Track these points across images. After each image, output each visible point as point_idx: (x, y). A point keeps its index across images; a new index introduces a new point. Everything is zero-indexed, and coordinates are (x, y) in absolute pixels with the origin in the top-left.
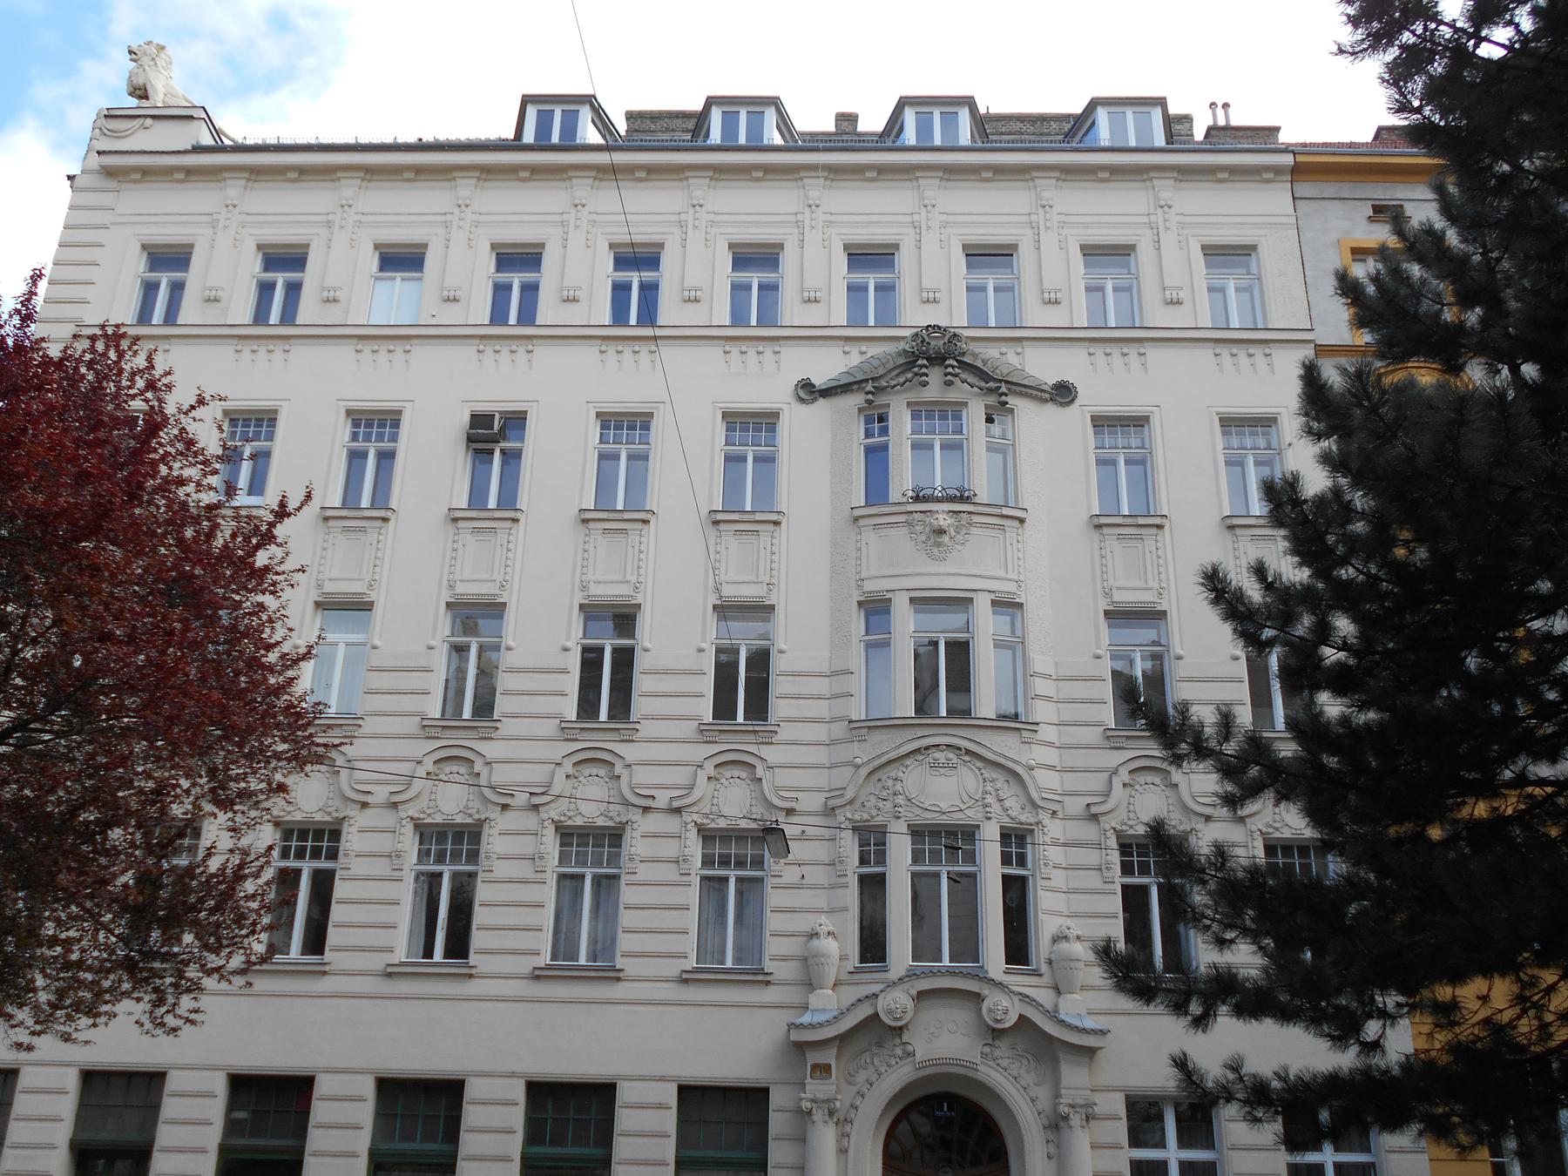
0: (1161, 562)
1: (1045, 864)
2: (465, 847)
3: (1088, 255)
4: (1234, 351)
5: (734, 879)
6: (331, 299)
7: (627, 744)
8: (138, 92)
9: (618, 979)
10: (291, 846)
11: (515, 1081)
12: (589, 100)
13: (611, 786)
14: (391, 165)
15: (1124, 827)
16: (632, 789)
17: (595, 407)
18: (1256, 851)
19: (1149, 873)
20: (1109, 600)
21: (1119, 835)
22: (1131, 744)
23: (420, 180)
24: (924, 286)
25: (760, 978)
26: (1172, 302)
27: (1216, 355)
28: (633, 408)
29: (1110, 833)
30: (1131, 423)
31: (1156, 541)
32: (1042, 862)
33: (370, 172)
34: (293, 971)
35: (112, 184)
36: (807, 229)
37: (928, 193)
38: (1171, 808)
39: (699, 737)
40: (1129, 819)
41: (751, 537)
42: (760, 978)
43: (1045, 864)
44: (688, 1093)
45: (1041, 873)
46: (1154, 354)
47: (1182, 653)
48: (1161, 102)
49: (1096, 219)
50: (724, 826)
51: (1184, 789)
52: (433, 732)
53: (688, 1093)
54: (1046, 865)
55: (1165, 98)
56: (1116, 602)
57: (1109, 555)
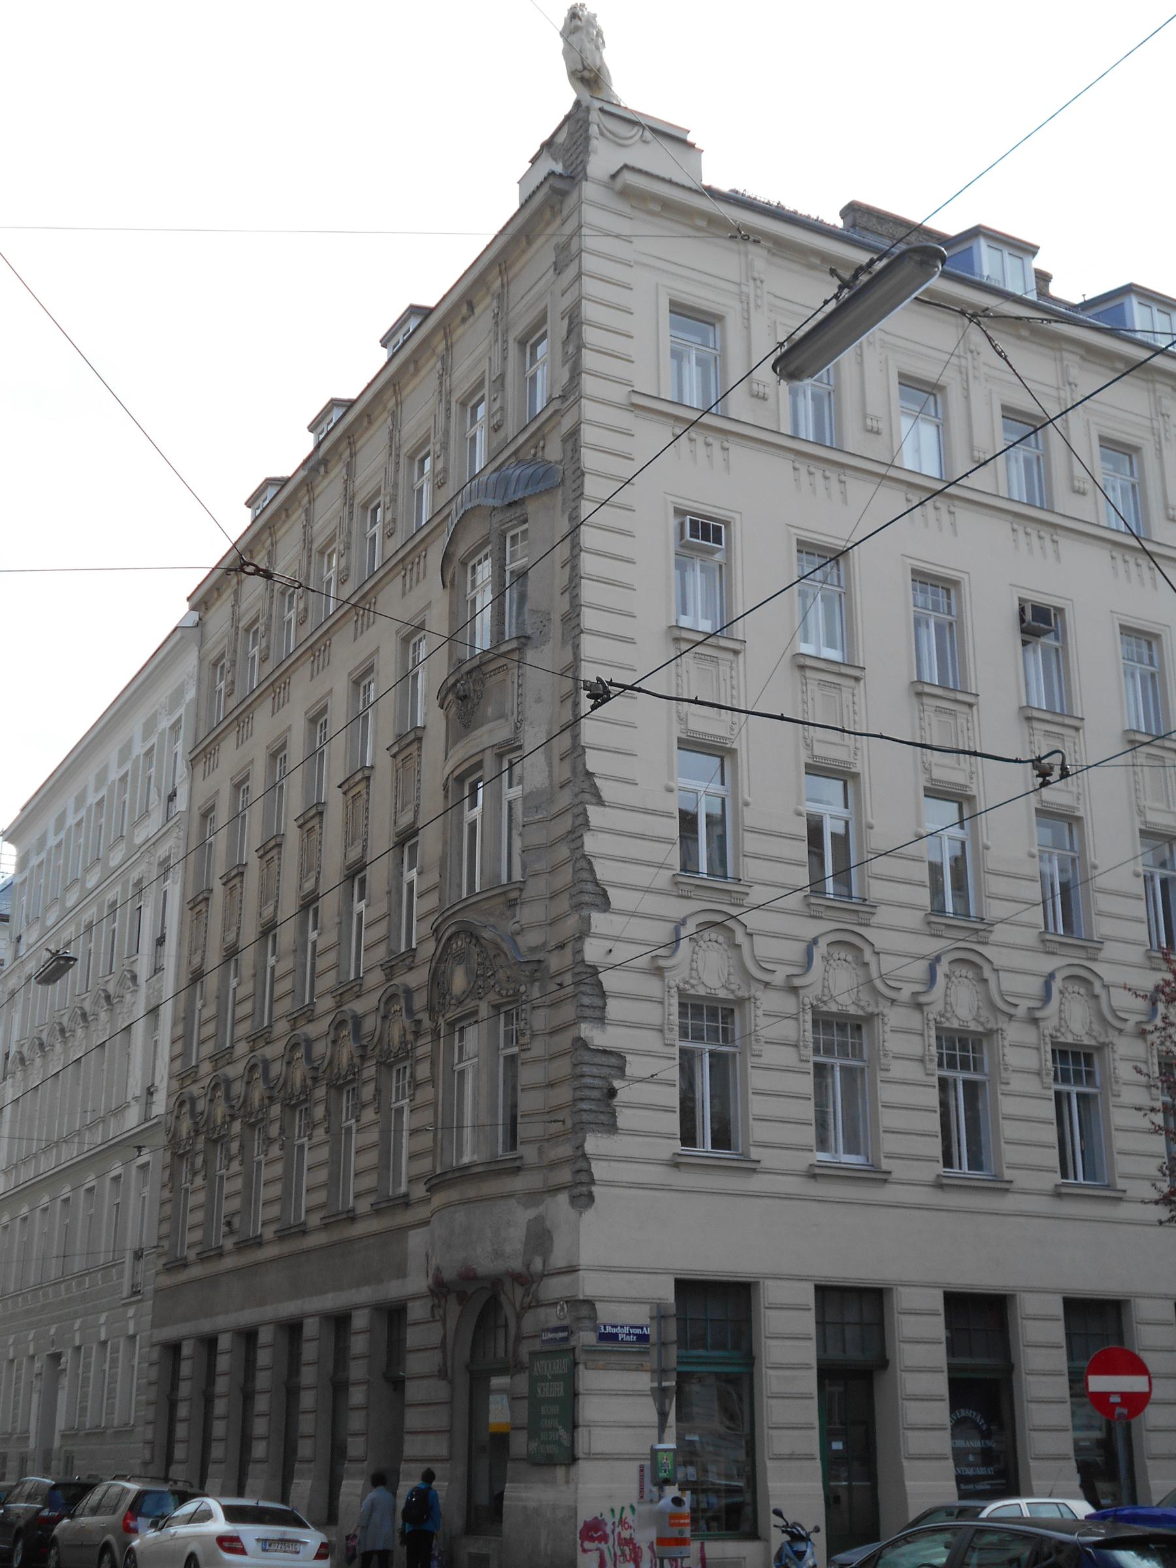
0: (735, 693)
1: (756, 1040)
2: (1071, 1068)
3: (1008, 418)
4: (710, 440)
5: (707, 1054)
6: (761, 395)
7: (815, 921)
8: (586, 74)
9: (754, 1170)
10: (702, 1020)
11: (664, 1277)
12: (1129, 289)
13: (730, 955)
14: (843, 259)
15: (687, 986)
16: (1002, 995)
17: (1118, 619)
18: (672, 1008)
19: (955, 1068)
20: (1143, 819)
21: (681, 993)
22: (1065, 951)
23: (667, 218)
24: (869, 411)
25: (999, 1185)
26: (871, 431)
27: (795, 469)
28: (702, 510)
29: (674, 991)
30: (816, 552)
31: (731, 668)
32: (1002, 1067)
33: (781, 246)
34: (830, 1176)
35: (624, 207)
36: (752, 305)
37: (1166, 402)
38: (732, 970)
39: (926, 930)
40: (691, 978)
41: (832, 690)
42: (999, 1185)
43: (756, 1040)
44: (824, 1292)
45: (751, 1049)
46: (1067, 545)
47: (989, 843)
48: (1030, 250)
49: (688, 273)
50: (704, 994)
51: (992, 984)
52: (1052, 947)
53: (824, 1292)
54: (885, 1055)
55: (1038, 248)
56: (1045, 802)
57: (927, 727)
